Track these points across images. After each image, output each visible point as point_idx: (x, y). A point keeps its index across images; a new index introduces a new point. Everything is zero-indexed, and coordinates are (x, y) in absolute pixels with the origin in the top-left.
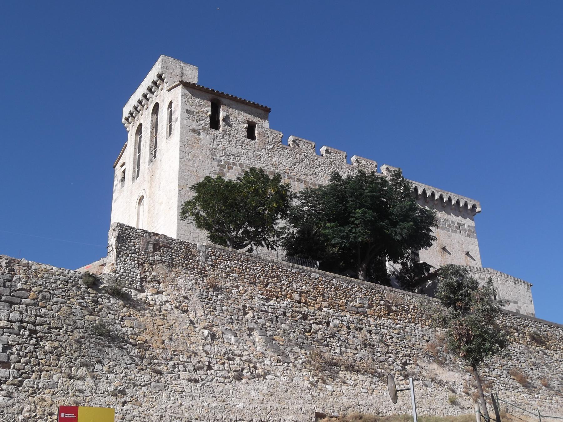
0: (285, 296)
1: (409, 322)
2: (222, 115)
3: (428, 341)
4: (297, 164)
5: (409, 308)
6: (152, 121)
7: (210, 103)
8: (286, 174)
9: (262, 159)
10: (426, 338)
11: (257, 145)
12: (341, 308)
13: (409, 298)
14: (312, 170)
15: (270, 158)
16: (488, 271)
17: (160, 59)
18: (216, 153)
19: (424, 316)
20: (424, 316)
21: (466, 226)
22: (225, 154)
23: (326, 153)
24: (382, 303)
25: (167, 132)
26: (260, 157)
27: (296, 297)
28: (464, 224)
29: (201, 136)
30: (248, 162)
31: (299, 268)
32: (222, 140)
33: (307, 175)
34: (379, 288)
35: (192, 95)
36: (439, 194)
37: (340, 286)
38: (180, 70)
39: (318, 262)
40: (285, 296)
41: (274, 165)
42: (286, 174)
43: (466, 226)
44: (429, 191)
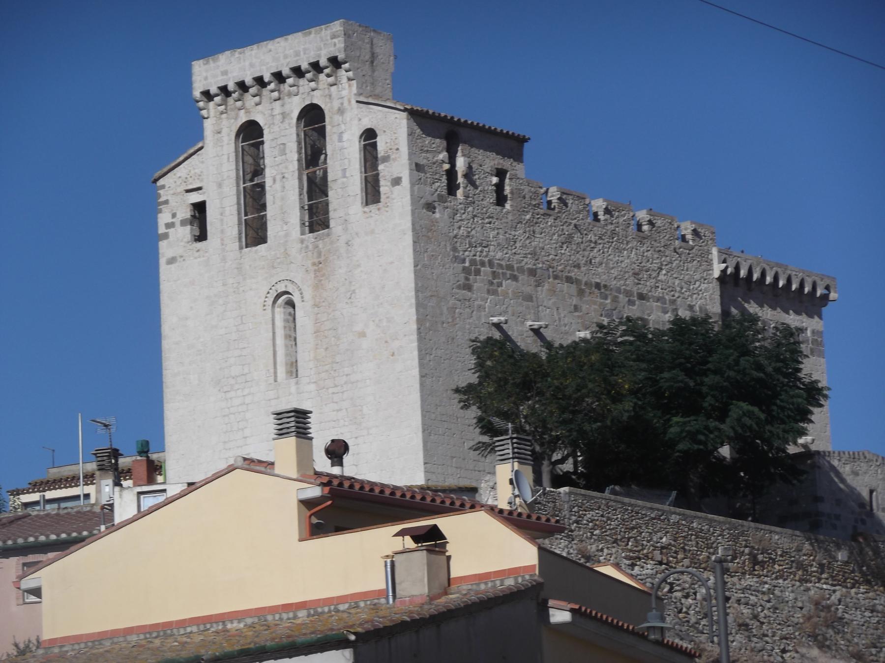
0: (646, 556)
1: (776, 578)
2: (461, 163)
3: (801, 608)
4: (565, 246)
5: (776, 555)
6: (298, 135)
7: (445, 143)
8: (551, 270)
9: (518, 245)
10: (800, 604)
11: (510, 217)
12: (703, 566)
13: (777, 537)
14: (586, 253)
15: (528, 242)
16: (865, 457)
17: (460, 148)
18: (458, 244)
19: (794, 565)
20: (794, 565)
21: (809, 333)
22: (471, 245)
23: (605, 214)
24: (747, 550)
25: (362, 189)
26: (515, 242)
27: (657, 555)
28: (806, 329)
29: (437, 215)
30: (499, 255)
31: (658, 510)
32: (464, 216)
33: (578, 266)
34: (742, 526)
35: (422, 130)
36: (773, 273)
37: (701, 531)
38: (368, 46)
39: (674, 493)
40: (646, 556)
41: (533, 254)
42: (551, 270)
43: (809, 333)
44: (758, 269)
